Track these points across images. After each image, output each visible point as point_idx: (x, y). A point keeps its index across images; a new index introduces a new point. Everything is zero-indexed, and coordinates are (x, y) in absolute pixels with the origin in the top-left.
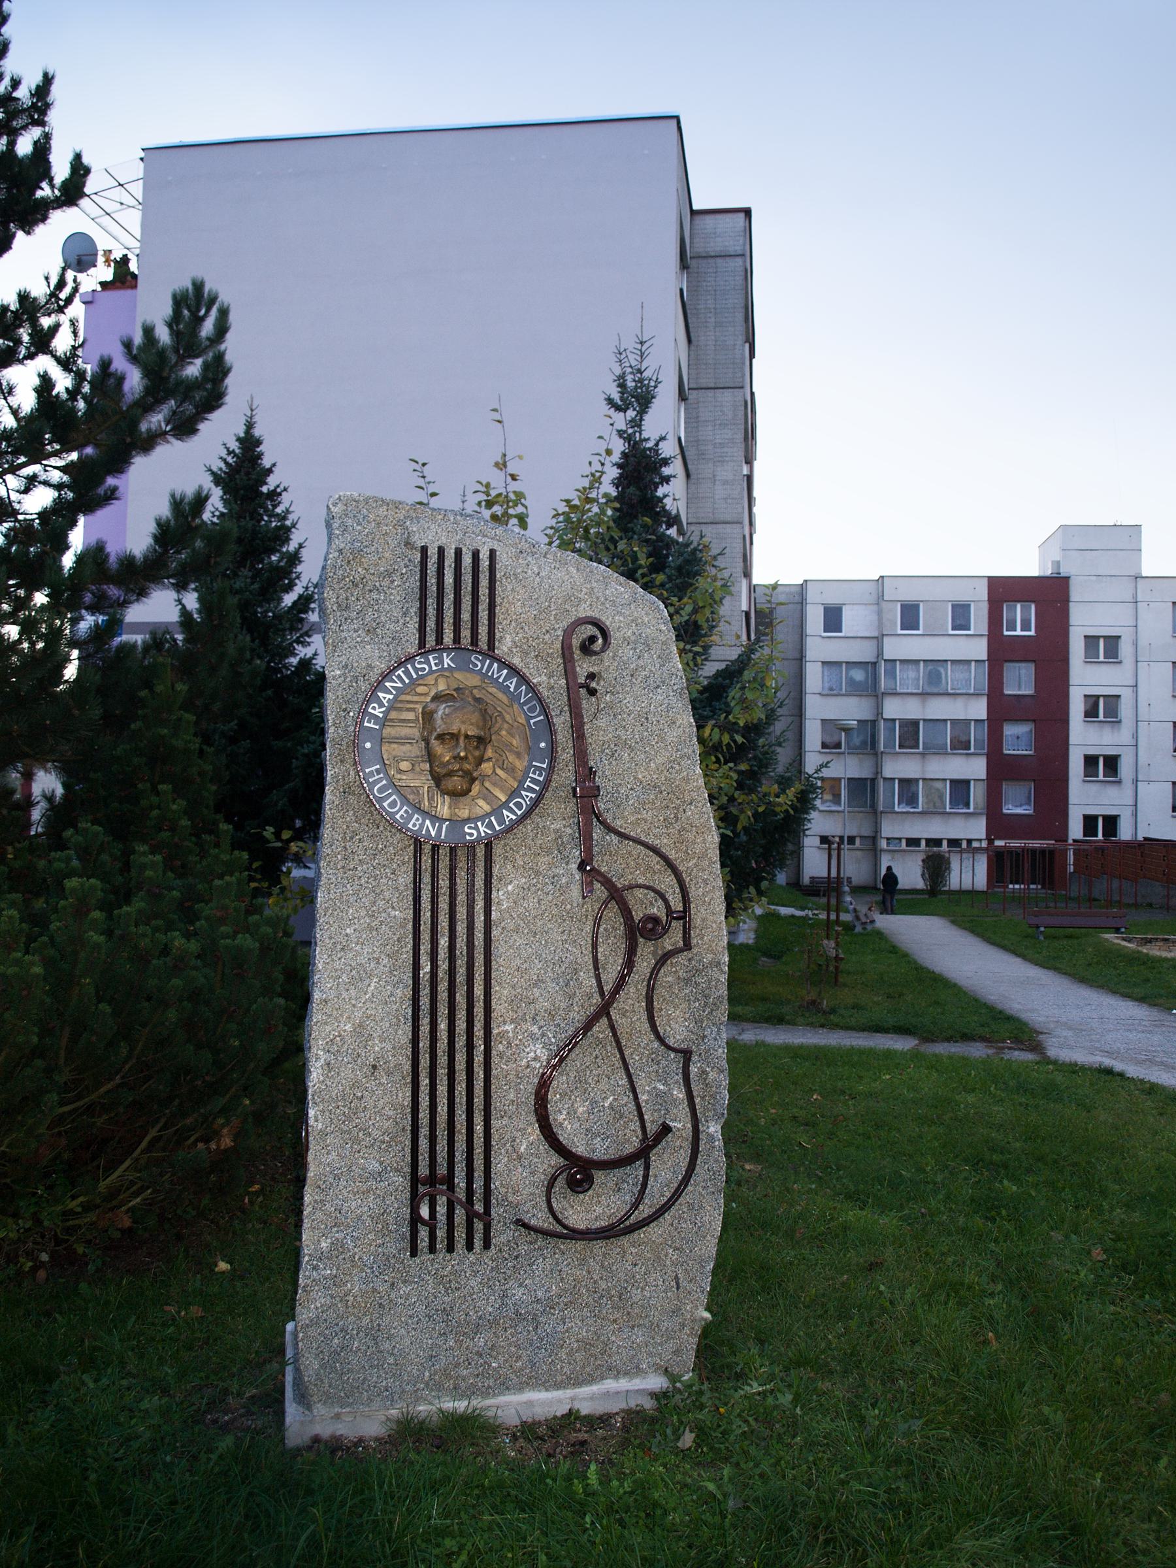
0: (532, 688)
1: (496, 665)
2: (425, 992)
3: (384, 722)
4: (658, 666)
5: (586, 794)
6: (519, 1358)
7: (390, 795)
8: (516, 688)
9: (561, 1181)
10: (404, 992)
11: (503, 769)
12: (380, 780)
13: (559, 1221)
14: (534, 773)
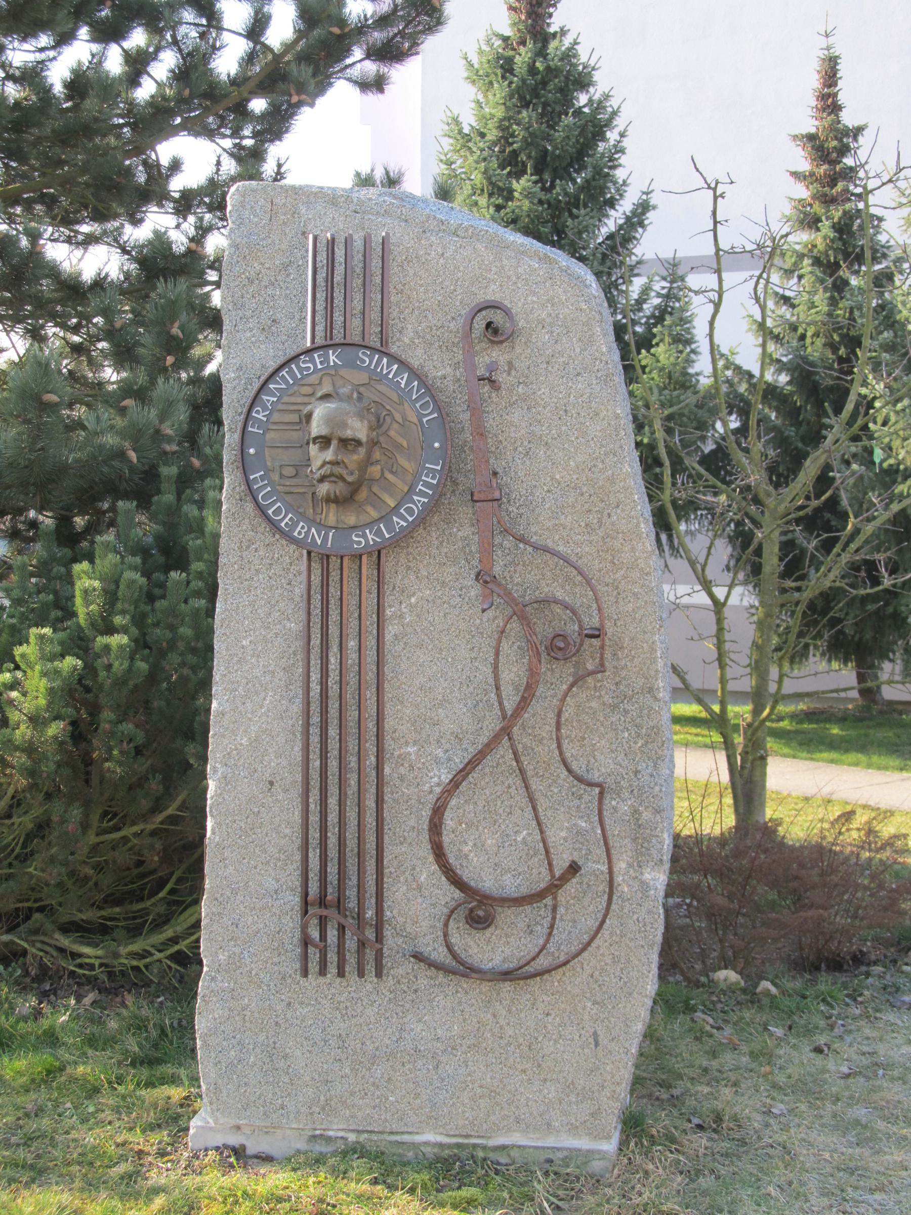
1: (385, 360)
2: (315, 708)
4: (578, 350)
6: (417, 1096)
7: (274, 503)
8: (274, 395)
9: (462, 913)
10: (297, 707)
11: (392, 472)
12: (265, 486)
13: (455, 956)
14: (427, 476)
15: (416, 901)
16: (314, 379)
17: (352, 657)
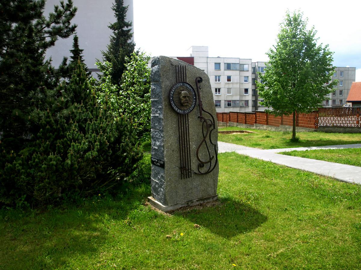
0: (193, 88)
3: (173, 94)
5: (200, 105)
13: (200, 172)
15: (194, 166)
16: (179, 87)
17: (183, 130)
